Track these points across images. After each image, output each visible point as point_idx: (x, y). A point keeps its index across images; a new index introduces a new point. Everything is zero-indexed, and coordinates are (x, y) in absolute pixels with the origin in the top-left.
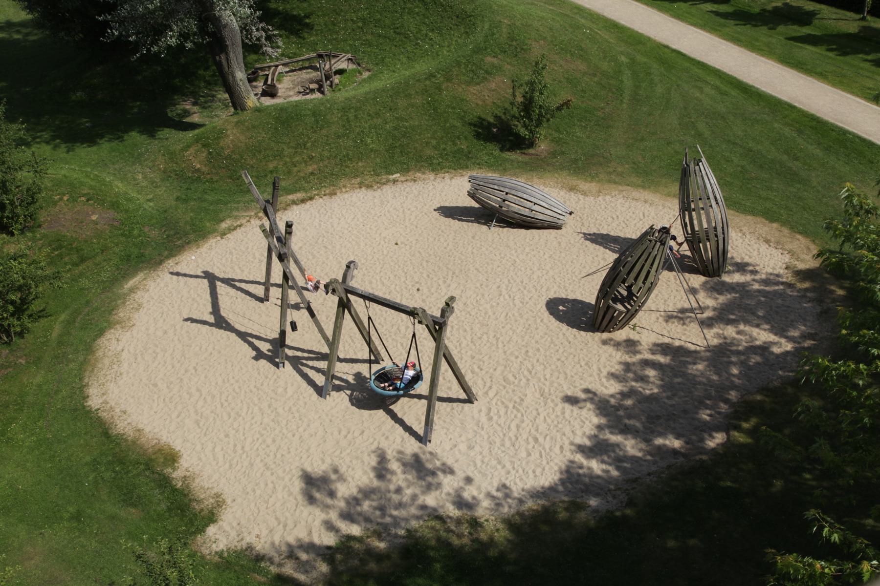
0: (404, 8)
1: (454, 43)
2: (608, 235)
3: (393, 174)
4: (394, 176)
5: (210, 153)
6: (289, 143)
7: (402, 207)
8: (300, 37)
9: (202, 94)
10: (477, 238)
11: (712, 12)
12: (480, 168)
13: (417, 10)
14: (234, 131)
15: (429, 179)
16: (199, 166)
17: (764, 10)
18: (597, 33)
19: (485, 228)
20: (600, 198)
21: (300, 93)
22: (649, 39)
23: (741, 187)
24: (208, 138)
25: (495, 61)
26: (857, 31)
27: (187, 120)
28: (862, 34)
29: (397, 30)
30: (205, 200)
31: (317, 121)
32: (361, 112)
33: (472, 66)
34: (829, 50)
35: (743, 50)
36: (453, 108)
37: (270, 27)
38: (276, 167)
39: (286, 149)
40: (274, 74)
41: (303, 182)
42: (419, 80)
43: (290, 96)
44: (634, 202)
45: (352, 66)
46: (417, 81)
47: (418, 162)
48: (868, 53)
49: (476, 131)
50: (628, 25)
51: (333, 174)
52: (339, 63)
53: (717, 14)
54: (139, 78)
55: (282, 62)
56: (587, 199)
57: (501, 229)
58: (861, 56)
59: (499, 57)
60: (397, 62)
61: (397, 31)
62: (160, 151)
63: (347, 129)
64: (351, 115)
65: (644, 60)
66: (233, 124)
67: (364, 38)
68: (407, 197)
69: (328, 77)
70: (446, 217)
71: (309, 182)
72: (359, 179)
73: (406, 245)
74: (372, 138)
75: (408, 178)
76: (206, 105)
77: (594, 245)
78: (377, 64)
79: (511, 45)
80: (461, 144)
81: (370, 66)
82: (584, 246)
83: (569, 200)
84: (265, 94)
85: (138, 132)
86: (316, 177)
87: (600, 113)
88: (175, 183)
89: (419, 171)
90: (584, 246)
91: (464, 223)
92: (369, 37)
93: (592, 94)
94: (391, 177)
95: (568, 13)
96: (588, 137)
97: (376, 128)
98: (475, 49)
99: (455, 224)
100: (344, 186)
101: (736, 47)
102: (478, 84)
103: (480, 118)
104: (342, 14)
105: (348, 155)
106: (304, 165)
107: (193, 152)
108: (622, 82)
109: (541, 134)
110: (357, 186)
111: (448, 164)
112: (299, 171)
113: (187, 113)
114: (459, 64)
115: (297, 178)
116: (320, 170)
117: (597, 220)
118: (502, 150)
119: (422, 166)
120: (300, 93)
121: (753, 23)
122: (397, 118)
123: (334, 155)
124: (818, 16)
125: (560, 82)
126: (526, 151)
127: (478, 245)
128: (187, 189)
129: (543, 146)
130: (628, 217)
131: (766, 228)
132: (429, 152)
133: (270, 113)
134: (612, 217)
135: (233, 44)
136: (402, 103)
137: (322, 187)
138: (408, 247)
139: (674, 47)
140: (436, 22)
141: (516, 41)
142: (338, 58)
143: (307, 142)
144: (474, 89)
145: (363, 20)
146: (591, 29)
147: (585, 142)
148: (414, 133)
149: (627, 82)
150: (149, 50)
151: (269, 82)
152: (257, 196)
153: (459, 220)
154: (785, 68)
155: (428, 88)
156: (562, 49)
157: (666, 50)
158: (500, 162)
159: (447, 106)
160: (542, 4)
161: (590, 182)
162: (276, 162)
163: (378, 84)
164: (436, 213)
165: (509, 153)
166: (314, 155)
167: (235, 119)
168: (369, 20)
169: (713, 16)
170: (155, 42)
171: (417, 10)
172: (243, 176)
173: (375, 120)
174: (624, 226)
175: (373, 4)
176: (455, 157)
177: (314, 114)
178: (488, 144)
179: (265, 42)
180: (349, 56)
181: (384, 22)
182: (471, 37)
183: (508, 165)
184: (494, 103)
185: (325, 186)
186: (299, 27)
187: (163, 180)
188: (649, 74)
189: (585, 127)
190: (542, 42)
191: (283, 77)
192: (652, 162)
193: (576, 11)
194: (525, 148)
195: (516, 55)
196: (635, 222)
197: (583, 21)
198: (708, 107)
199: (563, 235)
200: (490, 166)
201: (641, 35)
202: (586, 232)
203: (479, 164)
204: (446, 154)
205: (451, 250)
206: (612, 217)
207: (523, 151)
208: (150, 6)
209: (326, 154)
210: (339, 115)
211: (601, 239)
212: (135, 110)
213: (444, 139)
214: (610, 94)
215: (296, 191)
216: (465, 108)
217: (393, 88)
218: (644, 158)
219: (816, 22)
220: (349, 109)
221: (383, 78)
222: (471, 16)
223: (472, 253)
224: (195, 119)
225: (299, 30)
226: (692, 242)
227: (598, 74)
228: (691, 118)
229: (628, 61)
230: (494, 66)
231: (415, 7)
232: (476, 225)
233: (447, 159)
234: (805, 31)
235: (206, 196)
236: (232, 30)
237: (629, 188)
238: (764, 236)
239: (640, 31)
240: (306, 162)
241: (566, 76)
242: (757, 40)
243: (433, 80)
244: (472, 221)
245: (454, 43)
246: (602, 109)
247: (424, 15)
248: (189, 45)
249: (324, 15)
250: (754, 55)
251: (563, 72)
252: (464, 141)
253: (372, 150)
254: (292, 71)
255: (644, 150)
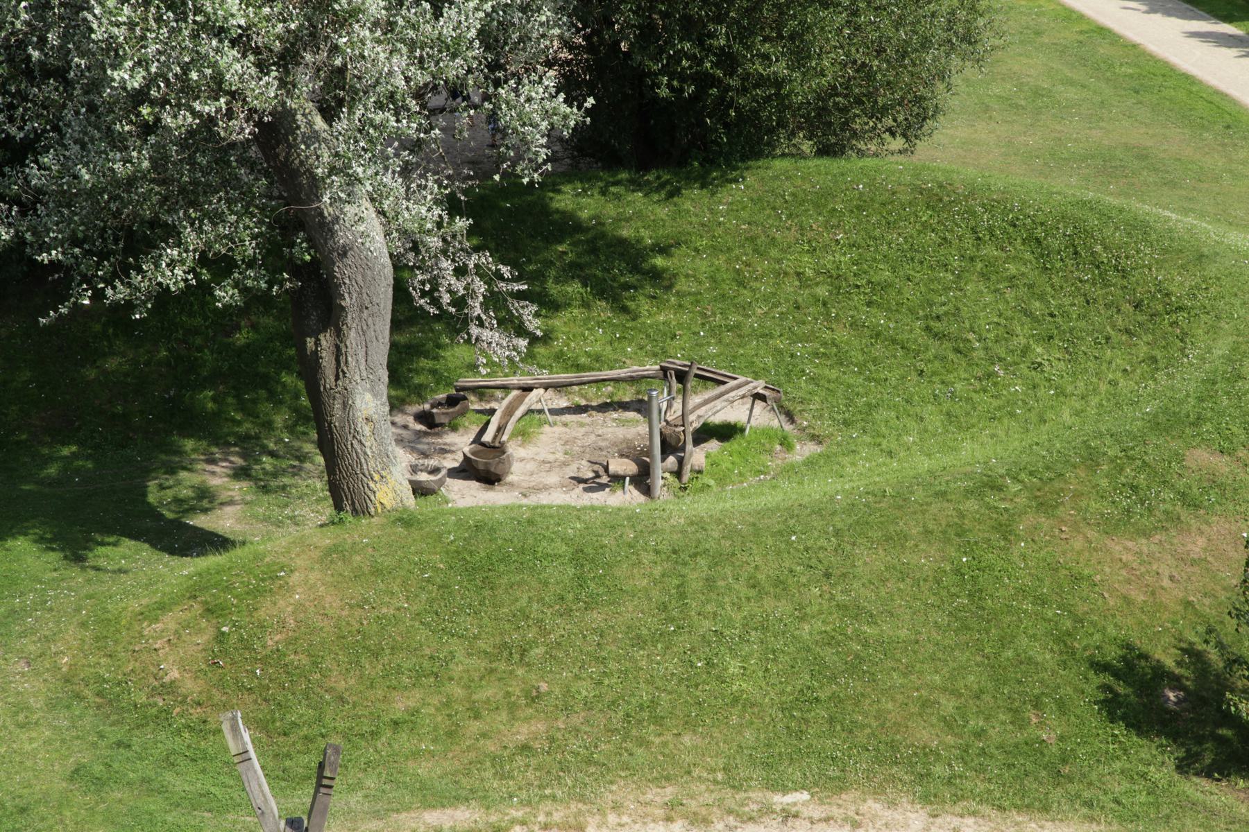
0: (972, 259)
1: (1103, 387)
3: (785, 790)
5: (220, 637)
6: (475, 637)
8: (625, 310)
9: (272, 446)
12: (1092, 819)
13: (1012, 269)
14: (314, 576)
16: (174, 674)
21: (580, 481)
24: (228, 588)
25: (1222, 465)
27: (200, 521)
30: (162, 790)
31: (580, 581)
32: (728, 571)
33: (1139, 470)
36: (1042, 601)
37: (505, 270)
38: (415, 712)
39: (460, 655)
40: (509, 412)
41: (488, 774)
42: (942, 494)
43: (546, 488)
45: (763, 417)
46: (937, 494)
47: (881, 764)
49: (1105, 688)
51: (589, 761)
52: (719, 404)
54: (91, 373)
55: (546, 376)
60: (911, 424)
61: (936, 326)
62: (78, 610)
63: (672, 620)
64: (695, 578)
66: (316, 554)
67: (827, 336)
69: (670, 446)
71: (503, 776)
72: (670, 791)
74: (745, 659)
75: (836, 812)
76: (274, 483)
78: (846, 423)
80: (1041, 725)
84: (468, 471)
85: (40, 540)
86: (534, 762)
88: (87, 721)
89: (879, 791)
92: (842, 334)
97: (765, 629)
98: (1162, 419)
100: (617, 807)
102: (1145, 534)
104: (774, 253)
105: (654, 702)
106: (504, 716)
107: (172, 626)
110: (660, 812)
111: (981, 787)
112: (484, 735)
113: (205, 498)
114: (1091, 459)
115: (472, 755)
116: (552, 740)
118: (1183, 767)
119: (893, 779)
120: (580, 481)
123: (608, 698)
128: (119, 744)
132: (926, 734)
133: (440, 536)
135: (364, 307)
136: (869, 560)
137: (543, 797)
140: (1066, 315)
142: (722, 388)
143: (534, 643)
144: (1123, 548)
145: (835, 278)
148: (890, 664)
150: (98, 295)
151: (488, 437)
152: (259, 801)
158: (1165, 811)
159: (1022, 591)
162: (417, 694)
163: (815, 489)
165: (1204, 783)
166: (544, 687)
167: (327, 539)
168: (852, 280)
170: (122, 272)
172: (226, 727)
173: (768, 603)
175: (877, 233)
176: (1010, 766)
177: (579, 557)
179: (478, 311)
180: (759, 386)
181: (899, 292)
182: (1160, 375)
185: (554, 798)
186: (628, 278)
187: (52, 705)
191: (542, 423)
203: (1089, 804)
204: (983, 752)
208: (118, 166)
209: (585, 689)
210: (657, 571)
212: (52, 470)
213: (987, 698)
215: (458, 800)
216: (1082, 608)
220: (695, 555)
221: (849, 470)
222: (1180, 309)
224: (222, 521)
225: (626, 287)
230: (1213, 481)
233: (981, 770)
235: (169, 777)
236: (367, 264)
240: (513, 708)
243: (992, 498)
247: (1030, 286)
248: (226, 295)
249: (715, 250)
252: (1052, 718)
253: (736, 700)
254: (578, 409)
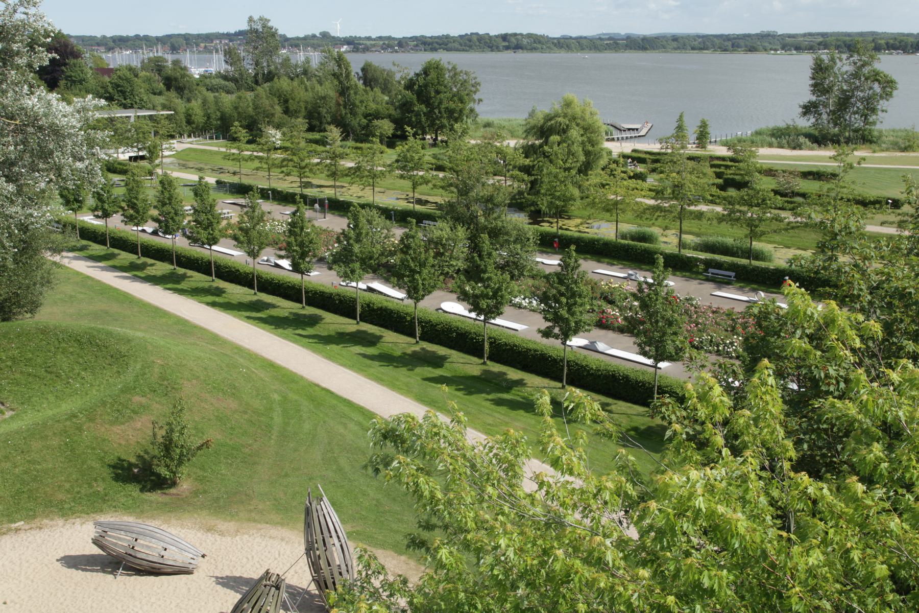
1: (105, 382)
2: (241, 577)
4: (17, 525)
7: (20, 559)
10: (99, 589)
11: (359, 354)
12: (116, 511)
13: (71, 350)
15: (58, 525)
17: (405, 354)
18: (253, 372)
19: (111, 577)
20: (237, 538)
22: (302, 378)
23: (375, 521)
25: (143, 400)
26: (479, 374)
28: (483, 377)
29: (48, 369)
33: (119, 405)
34: (456, 390)
35: (385, 389)
36: (94, 449)
42: (58, 421)
44: (271, 540)
46: (57, 421)
47: (46, 507)
48: (488, 393)
50: (283, 364)
53: (365, 356)
56: (224, 539)
57: (128, 577)
58: (483, 395)
59: (148, 396)
60: (45, 401)
65: (296, 397)
67: (12, 377)
68: (28, 547)
70: (69, 567)
73: (16, 603)
75: (33, 525)
77: (225, 589)
78: (22, 403)
79: (161, 385)
80: (97, 486)
81: (14, 406)
82: (214, 591)
83: (206, 541)
87: (247, 450)
89: (47, 517)
90: (214, 591)
91: (88, 573)
92: (18, 376)
93: (241, 431)
94: (13, 526)
95: (229, 353)
96: (233, 475)
99: (77, 575)
101: (380, 386)
102: (123, 423)
103: (119, 459)
108: (272, 418)
109: (182, 474)
111: (80, 508)
114: (104, 403)
117: (231, 561)
119: (52, 512)
121: (395, 364)
122: (29, 461)
124: (448, 360)
125: (209, 420)
126: (166, 491)
127: (100, 598)
129: (185, 485)
130: (263, 557)
131: (394, 562)
132: (61, 496)
134: (247, 558)
136: (36, 445)
138: (18, 606)
139: (324, 385)
140: (90, 362)
141: (168, 380)
144: (117, 429)
145: (13, 359)
146: (248, 368)
147: (229, 480)
148: (47, 476)
149: (278, 419)
153: (83, 570)
154: (421, 406)
155: (67, 429)
156: (214, 388)
157: (317, 388)
159: (87, 447)
160: (204, 344)
161: (229, 521)
163: (15, 426)
164: (58, 564)
165: (149, 494)
169: (361, 357)
171: (71, 350)
174: (259, 566)
178: (128, 485)
182: (121, 376)
183: (146, 507)
184: (138, 442)
188: (298, 411)
189: (231, 465)
190: (194, 381)
192: (293, 498)
193: (236, 351)
194: (167, 488)
195: (166, 394)
196: (270, 561)
197: (242, 360)
198: (351, 443)
199: (194, 581)
200: (127, 509)
201: (295, 374)
202: (219, 575)
203: (115, 507)
204: (80, 498)
205: (67, 606)
206: (247, 558)
207: (164, 491)
211: (229, 582)
214: (259, 431)
216: (106, 449)
217: (28, 430)
218: (286, 494)
219: (447, 365)
221: (25, 418)
223: (92, 607)
226: (318, 582)
227: (249, 411)
228: (333, 453)
229: (280, 398)
231: (70, 347)
232: (101, 574)
233: (80, 503)
234: (438, 372)
237: (268, 525)
238: (392, 569)
239: (294, 370)
241: (216, 414)
242: (397, 380)
243: (74, 420)
244: (97, 571)
245: (105, 382)
246: (250, 445)
250: (394, 393)
251: (213, 410)
252: (100, 483)
255: (286, 486)
